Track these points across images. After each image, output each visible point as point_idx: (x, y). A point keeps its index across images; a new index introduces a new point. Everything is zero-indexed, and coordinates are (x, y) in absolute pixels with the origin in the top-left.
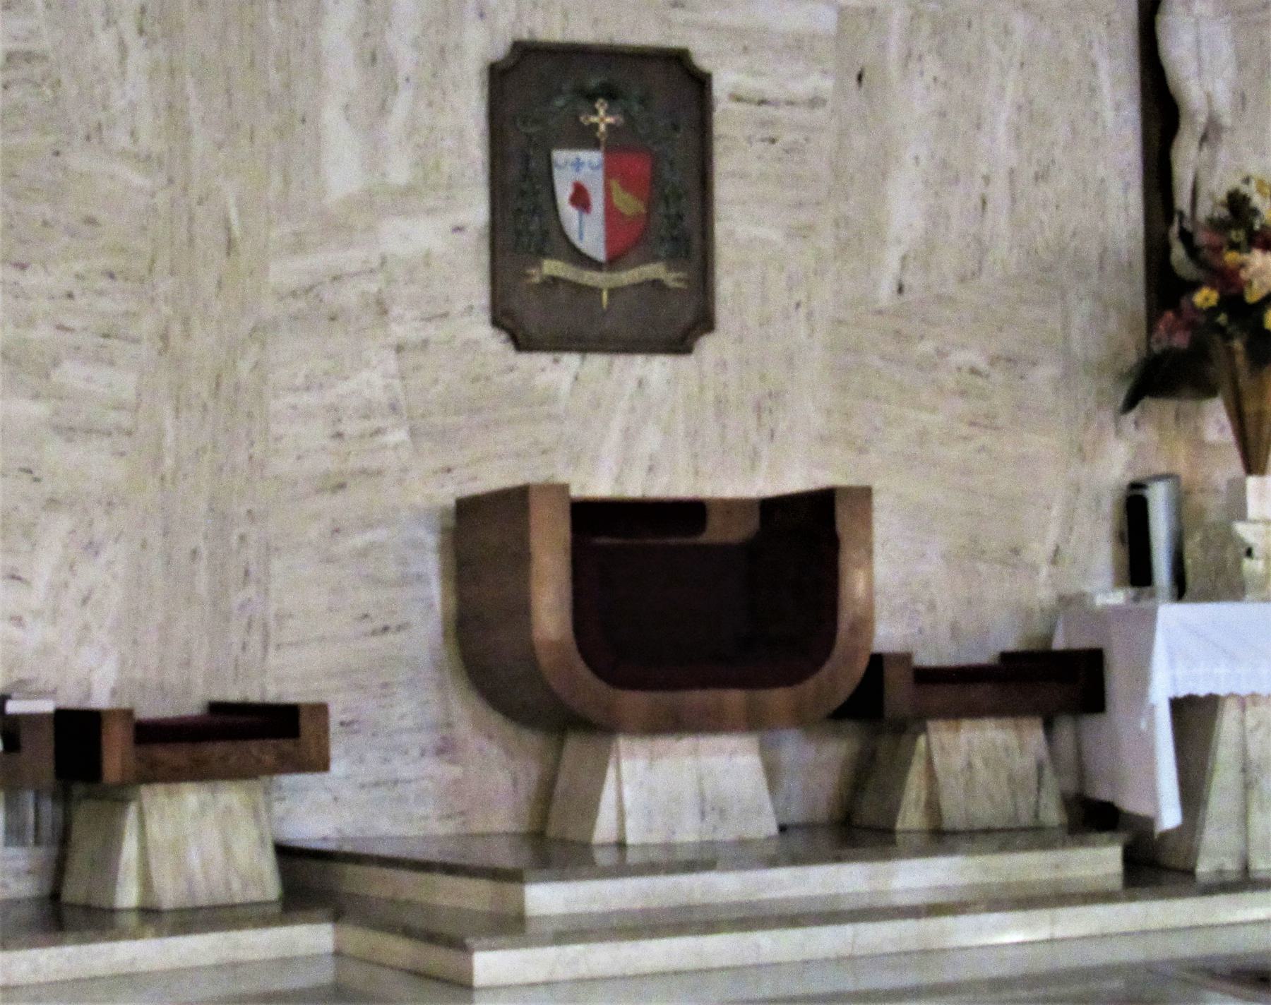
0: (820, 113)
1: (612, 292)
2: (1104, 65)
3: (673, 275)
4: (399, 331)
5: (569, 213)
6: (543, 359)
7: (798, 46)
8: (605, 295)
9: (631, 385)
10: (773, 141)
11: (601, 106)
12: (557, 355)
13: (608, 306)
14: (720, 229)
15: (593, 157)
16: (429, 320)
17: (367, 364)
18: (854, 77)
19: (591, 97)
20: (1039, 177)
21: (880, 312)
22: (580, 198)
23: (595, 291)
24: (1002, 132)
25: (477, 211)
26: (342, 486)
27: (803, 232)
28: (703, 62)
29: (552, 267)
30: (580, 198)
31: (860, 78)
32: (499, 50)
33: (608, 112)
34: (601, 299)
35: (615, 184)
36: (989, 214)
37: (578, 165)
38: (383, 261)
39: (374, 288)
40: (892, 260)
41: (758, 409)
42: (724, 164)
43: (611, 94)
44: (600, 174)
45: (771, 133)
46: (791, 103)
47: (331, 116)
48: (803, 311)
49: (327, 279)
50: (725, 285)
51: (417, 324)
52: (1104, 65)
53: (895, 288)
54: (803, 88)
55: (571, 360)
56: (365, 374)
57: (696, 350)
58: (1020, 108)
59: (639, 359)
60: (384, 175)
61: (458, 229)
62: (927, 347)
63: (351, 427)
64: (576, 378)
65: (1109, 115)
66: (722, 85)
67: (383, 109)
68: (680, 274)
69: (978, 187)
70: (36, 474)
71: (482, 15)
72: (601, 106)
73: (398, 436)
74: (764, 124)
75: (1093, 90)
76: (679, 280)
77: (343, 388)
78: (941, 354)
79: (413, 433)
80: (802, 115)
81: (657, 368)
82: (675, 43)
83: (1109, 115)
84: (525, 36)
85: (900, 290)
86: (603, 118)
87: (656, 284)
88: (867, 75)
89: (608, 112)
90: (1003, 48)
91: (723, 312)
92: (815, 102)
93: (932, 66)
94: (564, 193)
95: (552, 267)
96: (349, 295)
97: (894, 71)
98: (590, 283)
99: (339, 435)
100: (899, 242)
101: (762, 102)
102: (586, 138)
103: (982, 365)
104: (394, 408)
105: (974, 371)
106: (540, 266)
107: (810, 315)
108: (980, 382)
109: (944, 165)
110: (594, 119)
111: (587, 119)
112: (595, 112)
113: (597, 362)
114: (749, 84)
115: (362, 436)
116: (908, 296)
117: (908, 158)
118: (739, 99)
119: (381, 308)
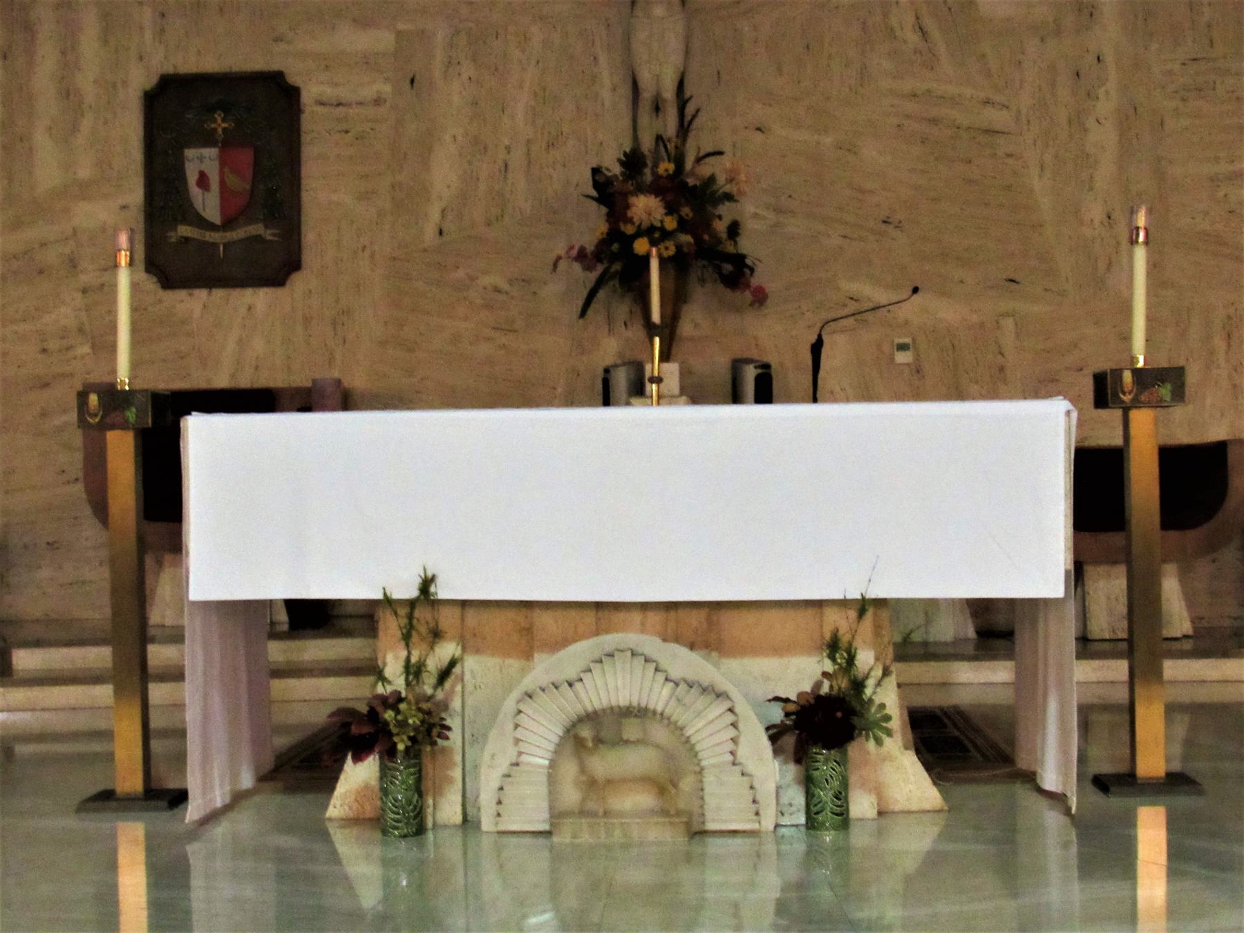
0: (383, 110)
1: (225, 245)
2: (603, 59)
3: (269, 232)
4: (84, 278)
5: (195, 191)
6: (182, 294)
7: (368, 62)
8: (221, 248)
9: (243, 310)
10: (347, 132)
11: (219, 116)
12: (190, 291)
13: (881, 726)
14: (306, 197)
15: (211, 153)
16: (105, 270)
17: (63, 302)
18: (408, 81)
19: (211, 110)
20: (551, 145)
21: (425, 250)
22: (203, 181)
23: (214, 245)
24: (520, 115)
25: (135, 194)
26: (46, 385)
27: (365, 196)
28: (293, 79)
29: (184, 230)
30: (203, 181)
31: (412, 81)
32: (151, 82)
33: (224, 120)
34: (219, 250)
35: (226, 170)
36: (510, 175)
37: (201, 159)
38: (75, 231)
39: (67, 251)
40: (435, 215)
41: (334, 324)
42: (310, 151)
43: (226, 108)
44: (216, 164)
45: (345, 126)
46: (361, 104)
47: (41, 139)
48: (367, 253)
49: (36, 246)
50: (309, 236)
51: (97, 273)
52: (603, 59)
53: (437, 232)
54: (368, 92)
55: (201, 294)
56: (63, 309)
57: (288, 283)
58: (536, 94)
59: (249, 292)
60: (75, 173)
61: (124, 207)
62: (460, 274)
63: (53, 345)
64: (205, 306)
65: (606, 94)
66: (310, 93)
67: (75, 129)
68: (276, 231)
69: (502, 155)
70: (731, 758)
71: (141, 58)
72: (219, 116)
73: (86, 349)
74: (339, 120)
75: (594, 79)
76: (274, 235)
77: (48, 319)
78: (472, 279)
79: (93, 347)
80: (371, 111)
81: (260, 298)
82: (275, 66)
83: (606, 94)
84: (171, 70)
85: (441, 233)
86: (220, 123)
87: (258, 239)
88: (417, 78)
89: (224, 120)
90: (523, 51)
91: (308, 257)
92: (378, 102)
93: (468, 70)
94: (192, 178)
95: (184, 230)
96: (51, 257)
97: (437, 73)
98: (211, 240)
99: (44, 351)
100: (441, 198)
101: (339, 105)
102: (207, 140)
103: (505, 286)
104: (81, 330)
105: (497, 290)
106: (176, 230)
107: (372, 256)
108: (502, 297)
109: (476, 141)
110: (220, 131)
111: (220, 136)
112: (215, 121)
113: (219, 293)
114: (329, 92)
115: (60, 351)
116: (446, 238)
117: (448, 138)
118: (322, 104)
119: (73, 264)
